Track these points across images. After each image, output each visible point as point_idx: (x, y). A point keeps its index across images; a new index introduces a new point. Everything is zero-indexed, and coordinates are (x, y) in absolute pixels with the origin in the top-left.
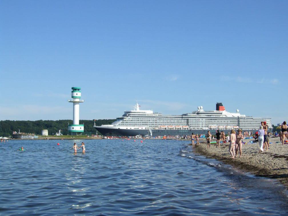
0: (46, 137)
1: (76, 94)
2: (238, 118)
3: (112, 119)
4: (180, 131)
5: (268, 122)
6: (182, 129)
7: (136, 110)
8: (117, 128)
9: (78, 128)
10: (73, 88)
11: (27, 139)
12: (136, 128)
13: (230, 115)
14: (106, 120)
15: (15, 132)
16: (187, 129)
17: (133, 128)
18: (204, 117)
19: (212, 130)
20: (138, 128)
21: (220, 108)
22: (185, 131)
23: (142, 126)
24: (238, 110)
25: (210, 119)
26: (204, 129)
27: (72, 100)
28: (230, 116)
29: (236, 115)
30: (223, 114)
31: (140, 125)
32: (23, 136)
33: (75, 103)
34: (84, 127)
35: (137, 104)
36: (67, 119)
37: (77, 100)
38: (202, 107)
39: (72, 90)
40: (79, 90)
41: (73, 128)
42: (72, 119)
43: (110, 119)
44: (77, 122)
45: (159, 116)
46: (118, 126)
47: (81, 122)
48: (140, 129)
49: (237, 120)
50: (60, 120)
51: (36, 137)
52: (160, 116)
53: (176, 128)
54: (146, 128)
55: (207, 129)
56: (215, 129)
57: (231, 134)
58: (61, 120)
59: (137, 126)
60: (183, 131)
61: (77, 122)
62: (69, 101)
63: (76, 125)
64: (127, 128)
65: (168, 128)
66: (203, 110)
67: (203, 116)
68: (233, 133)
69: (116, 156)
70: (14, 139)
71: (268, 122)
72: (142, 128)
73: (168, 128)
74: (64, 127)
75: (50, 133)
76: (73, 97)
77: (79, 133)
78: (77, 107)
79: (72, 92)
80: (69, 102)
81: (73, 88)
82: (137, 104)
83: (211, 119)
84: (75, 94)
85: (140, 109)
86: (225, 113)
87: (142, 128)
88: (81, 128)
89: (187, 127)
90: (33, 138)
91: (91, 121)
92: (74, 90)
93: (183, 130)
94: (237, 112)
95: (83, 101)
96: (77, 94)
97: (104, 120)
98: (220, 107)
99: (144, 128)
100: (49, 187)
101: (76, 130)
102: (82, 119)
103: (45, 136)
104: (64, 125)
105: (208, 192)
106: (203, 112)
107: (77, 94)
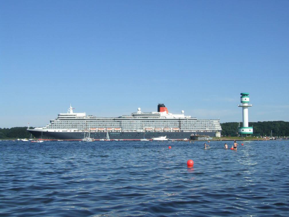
0: (219, 139)
1: (244, 99)
2: (180, 119)
3: (277, 121)
4: (111, 134)
5: (215, 123)
6: (113, 132)
7: (69, 112)
8: (45, 130)
9: (248, 130)
10: (241, 94)
11: (203, 141)
12: (65, 131)
13: (170, 116)
14: (271, 121)
15: (193, 134)
16: (118, 132)
17: (61, 131)
18: (139, 118)
19: (147, 132)
20: (67, 131)
21: (161, 110)
22: (117, 134)
23: (71, 129)
24: (183, 111)
25: (147, 121)
26: (139, 131)
27: (241, 105)
28: (170, 117)
29: (177, 116)
30: (161, 116)
31: (69, 128)
32: (199, 138)
33: (244, 107)
34: (253, 130)
35: (71, 107)
36: (233, 122)
37: (246, 105)
38: (139, 109)
39: (241, 96)
40: (247, 95)
41: (243, 130)
42: (242, 122)
43: (275, 121)
44: (246, 124)
45: (90, 119)
46: (46, 129)
47: (250, 124)
48: (69, 131)
49: (178, 121)
50: (226, 123)
51: (211, 138)
52: (91, 119)
53: (115, 131)
54: (75, 131)
55: (142, 131)
56: (151, 132)
57: (215, 136)
58: (227, 122)
59: (65, 129)
60: (115, 134)
61: (246, 124)
62: (239, 105)
63: (245, 128)
64: (55, 131)
65: (114, 131)
66: (140, 112)
67: (138, 118)
68: (215, 134)
69: (9, 158)
70: (192, 140)
71: (215, 123)
72: (71, 131)
73: (173, 130)
74: (231, 129)
75: (255, 137)
76: (242, 102)
77: (249, 135)
78: (246, 111)
79: (241, 97)
80: (239, 106)
81: (241, 94)
82: (71, 107)
83: (148, 121)
84: (244, 99)
85: (74, 112)
86: (163, 114)
87: (71, 131)
88: (250, 130)
89: (178, 130)
90: (208, 139)
91: (256, 123)
92: (243, 95)
93: (114, 133)
94: (182, 113)
95: (251, 105)
96: (247, 99)
97: (269, 122)
98: (161, 108)
99: (72, 131)
100: (152, 188)
101: (246, 132)
102: (249, 122)
103: (219, 138)
104: (230, 127)
105: (153, 201)
106: (142, 114)
107: (245, 99)
